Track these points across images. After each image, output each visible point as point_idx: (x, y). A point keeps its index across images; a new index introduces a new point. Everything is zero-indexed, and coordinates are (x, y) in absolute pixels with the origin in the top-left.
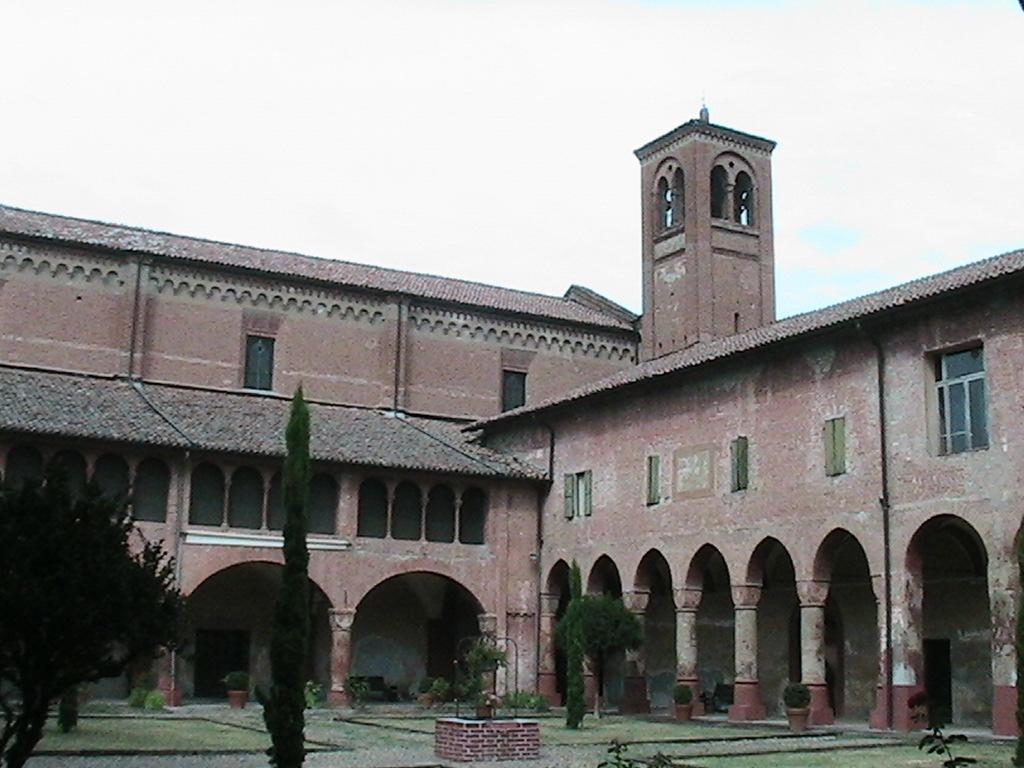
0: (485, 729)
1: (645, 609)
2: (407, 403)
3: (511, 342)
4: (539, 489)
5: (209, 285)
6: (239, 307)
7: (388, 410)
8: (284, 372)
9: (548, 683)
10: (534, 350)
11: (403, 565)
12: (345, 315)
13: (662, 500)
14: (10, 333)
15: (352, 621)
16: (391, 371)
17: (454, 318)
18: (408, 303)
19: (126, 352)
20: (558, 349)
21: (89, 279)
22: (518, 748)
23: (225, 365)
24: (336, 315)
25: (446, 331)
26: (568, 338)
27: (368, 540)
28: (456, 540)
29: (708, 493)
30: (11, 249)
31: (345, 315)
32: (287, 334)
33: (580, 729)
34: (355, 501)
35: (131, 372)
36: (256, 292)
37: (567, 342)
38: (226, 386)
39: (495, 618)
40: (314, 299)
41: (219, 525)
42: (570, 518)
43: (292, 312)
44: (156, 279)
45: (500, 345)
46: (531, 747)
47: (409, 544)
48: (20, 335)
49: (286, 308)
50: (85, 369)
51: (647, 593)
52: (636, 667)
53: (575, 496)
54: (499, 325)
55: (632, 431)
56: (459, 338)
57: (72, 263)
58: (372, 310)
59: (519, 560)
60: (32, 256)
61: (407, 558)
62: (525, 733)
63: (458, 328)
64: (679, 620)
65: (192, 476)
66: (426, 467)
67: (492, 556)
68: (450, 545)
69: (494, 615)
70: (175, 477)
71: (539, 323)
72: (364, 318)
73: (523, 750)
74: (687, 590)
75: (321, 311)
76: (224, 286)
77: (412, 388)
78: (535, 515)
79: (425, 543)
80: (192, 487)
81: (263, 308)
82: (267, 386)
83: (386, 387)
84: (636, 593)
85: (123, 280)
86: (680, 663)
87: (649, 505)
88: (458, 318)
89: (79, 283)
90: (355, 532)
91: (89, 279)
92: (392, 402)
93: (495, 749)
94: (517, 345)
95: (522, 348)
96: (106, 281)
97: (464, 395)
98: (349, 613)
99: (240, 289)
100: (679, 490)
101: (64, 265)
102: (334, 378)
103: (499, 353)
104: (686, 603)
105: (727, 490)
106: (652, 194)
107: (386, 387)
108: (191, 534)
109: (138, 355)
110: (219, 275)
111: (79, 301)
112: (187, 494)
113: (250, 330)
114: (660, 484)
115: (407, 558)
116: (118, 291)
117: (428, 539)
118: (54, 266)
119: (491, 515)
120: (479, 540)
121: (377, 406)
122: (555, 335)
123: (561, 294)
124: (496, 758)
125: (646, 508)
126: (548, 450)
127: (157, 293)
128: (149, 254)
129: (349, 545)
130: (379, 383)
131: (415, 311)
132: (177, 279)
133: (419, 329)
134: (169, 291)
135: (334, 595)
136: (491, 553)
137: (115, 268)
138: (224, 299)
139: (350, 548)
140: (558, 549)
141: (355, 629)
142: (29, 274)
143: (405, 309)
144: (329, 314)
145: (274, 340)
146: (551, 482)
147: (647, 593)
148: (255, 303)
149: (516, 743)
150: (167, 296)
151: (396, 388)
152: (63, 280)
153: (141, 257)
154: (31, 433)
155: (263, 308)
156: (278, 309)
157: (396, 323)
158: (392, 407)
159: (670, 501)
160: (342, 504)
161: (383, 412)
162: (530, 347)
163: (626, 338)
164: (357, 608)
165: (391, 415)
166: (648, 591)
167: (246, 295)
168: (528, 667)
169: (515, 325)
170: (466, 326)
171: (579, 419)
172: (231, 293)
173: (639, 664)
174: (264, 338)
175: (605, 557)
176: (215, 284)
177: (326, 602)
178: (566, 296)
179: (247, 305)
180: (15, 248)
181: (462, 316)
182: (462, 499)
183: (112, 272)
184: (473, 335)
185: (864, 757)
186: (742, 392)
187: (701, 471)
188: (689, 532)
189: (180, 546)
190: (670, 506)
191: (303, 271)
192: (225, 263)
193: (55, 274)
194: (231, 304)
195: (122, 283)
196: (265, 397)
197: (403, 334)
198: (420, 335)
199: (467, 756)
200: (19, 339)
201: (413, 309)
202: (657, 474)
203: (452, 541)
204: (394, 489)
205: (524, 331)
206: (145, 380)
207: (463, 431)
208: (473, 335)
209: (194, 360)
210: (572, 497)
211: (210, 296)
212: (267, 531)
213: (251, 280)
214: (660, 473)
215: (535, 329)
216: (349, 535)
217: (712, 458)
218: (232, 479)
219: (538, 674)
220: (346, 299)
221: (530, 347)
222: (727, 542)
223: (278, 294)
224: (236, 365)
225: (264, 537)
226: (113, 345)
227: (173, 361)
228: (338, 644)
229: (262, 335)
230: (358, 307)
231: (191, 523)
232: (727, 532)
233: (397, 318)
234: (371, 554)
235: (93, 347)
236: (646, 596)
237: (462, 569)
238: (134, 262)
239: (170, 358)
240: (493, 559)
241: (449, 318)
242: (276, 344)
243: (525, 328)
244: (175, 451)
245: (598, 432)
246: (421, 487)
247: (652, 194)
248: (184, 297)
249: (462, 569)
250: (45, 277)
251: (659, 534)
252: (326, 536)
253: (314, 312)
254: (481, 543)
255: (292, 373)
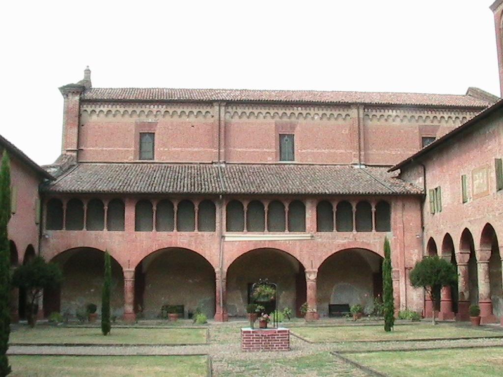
0: (254, 334)
1: (468, 262)
2: (366, 159)
3: (425, 121)
4: (420, 199)
5: (256, 112)
6: (273, 121)
7: (356, 164)
8: (299, 151)
9: (429, 303)
10: (439, 124)
11: (343, 245)
12: (329, 118)
13: (468, 200)
14: (161, 147)
15: (316, 276)
16: (356, 144)
17: (102, 108)
18: (362, 108)
19: (216, 149)
20: (452, 122)
21: (196, 117)
22: (275, 345)
23: (267, 150)
24: (325, 119)
25: (386, 120)
26: (457, 115)
27: (183, 233)
28: (374, 230)
29: (486, 193)
30: (158, 107)
31: (329, 118)
32: (299, 131)
33: (394, 332)
34: (315, 213)
35: (219, 159)
36: (281, 112)
37: (457, 118)
38: (270, 161)
39: (398, 271)
40: (312, 111)
41: (243, 231)
42: (434, 214)
43: (301, 120)
44: (229, 112)
45: (418, 124)
46: (284, 344)
47: (347, 234)
48: (166, 147)
49: (297, 118)
50: (198, 160)
51: (468, 253)
52: (463, 294)
53: (435, 202)
54: (416, 113)
55: (454, 162)
56: (394, 123)
57: (187, 110)
58: (344, 114)
59: (411, 238)
60: (185, 110)
61: (345, 241)
62: (280, 336)
63: (393, 117)
64: (479, 267)
65: (227, 208)
66: (351, 192)
67: (394, 237)
68: (171, 233)
69: (397, 269)
70: (217, 208)
71: (440, 110)
72: (340, 119)
73: (278, 346)
74: (481, 250)
75: (316, 117)
76: (264, 111)
77: (370, 152)
78: (419, 213)
79: (355, 232)
80: (227, 210)
81: (285, 119)
82: (151, 157)
83: (354, 153)
84: (461, 253)
85: (213, 115)
86: (480, 292)
87: (464, 202)
88: (392, 112)
89: (192, 119)
90: (316, 230)
91: (196, 117)
92: (358, 160)
93: (261, 345)
94: (428, 123)
95: (432, 124)
96: (205, 116)
97: (399, 153)
98: (314, 272)
99: (272, 112)
100: (475, 194)
101: (421, 116)
102: (327, 151)
103: (418, 128)
104: (481, 258)
105: (495, 190)
106: (500, 29)
107: (354, 153)
108: (228, 237)
109: (222, 151)
110: (261, 106)
111: (193, 128)
112: (224, 217)
113: (281, 132)
114: (467, 191)
115: (345, 241)
116: (212, 120)
117: (338, 231)
118: (179, 113)
119: (393, 215)
120: (387, 228)
121: (351, 163)
122: (449, 115)
123: (464, 93)
124: (261, 350)
125: (462, 205)
126: (423, 177)
127: (231, 119)
128: (223, 101)
129: (312, 236)
130: (351, 151)
131: (368, 111)
132: (240, 111)
133: (371, 121)
134: (237, 117)
135: (306, 264)
136: (394, 236)
137: (209, 109)
138: (264, 117)
139: (313, 238)
140: (429, 233)
141: (318, 278)
142: (168, 118)
143: (223, 109)
144: (321, 119)
145: (294, 135)
146: (426, 195)
147: (468, 253)
148: (281, 118)
149: (273, 342)
150: (236, 119)
151: (360, 152)
152: (184, 118)
153: (356, 105)
154: (191, 194)
155: (285, 119)
156: (293, 119)
157: (357, 119)
158: (358, 163)
159: (472, 199)
160: (307, 216)
161: (353, 166)
162: (436, 123)
163: (447, 110)
164: (318, 269)
165: (358, 167)
166: (470, 252)
167: (117, 112)
168: (420, 296)
169: (426, 112)
170: (397, 116)
171: (434, 159)
172: (268, 114)
173: (465, 294)
174: (430, 138)
175: (447, 234)
176: (259, 111)
177: (302, 268)
178: (467, 93)
179: (277, 119)
180: (160, 106)
181: (156, 106)
182: (375, 208)
183: (207, 112)
184: (402, 120)
185: (336, 356)
186: (498, 132)
187: (483, 181)
188: (480, 217)
189: (222, 243)
190: (472, 202)
191: (264, 98)
192: (335, 101)
193: (180, 116)
194: (269, 120)
195: (213, 116)
196: (290, 164)
197: (361, 124)
198: (372, 124)
199: (244, 349)
200: (166, 149)
201: (366, 110)
202: (465, 186)
203: (371, 231)
204: (336, 206)
205: (431, 115)
206: (227, 162)
207: (389, 171)
208: (402, 120)
209: (252, 150)
210: (434, 202)
211: (257, 117)
212: (268, 232)
213: (331, 107)
214: (467, 184)
215: (438, 113)
216: (312, 231)
217: (487, 172)
218: (356, 207)
219: (425, 300)
220: (329, 109)
221: (436, 123)
222: (496, 221)
223: (292, 111)
224: (273, 150)
225: (265, 235)
226: (210, 147)
227: (303, 152)
228: (309, 288)
229: (287, 133)
230: (336, 113)
231: (227, 231)
232: (495, 215)
233: (357, 116)
234: (325, 240)
235: (202, 149)
236: (469, 255)
237: (378, 246)
238: (216, 105)
239: (239, 150)
240: (395, 239)
241: (387, 113)
242: (295, 137)
243: (432, 113)
244: (215, 196)
245: (442, 165)
246: (103, 202)
247: (500, 29)
248: (244, 119)
249: (378, 246)
250: (176, 119)
251: (468, 219)
252: (300, 233)
253: (313, 118)
254: (390, 231)
255: (303, 151)
